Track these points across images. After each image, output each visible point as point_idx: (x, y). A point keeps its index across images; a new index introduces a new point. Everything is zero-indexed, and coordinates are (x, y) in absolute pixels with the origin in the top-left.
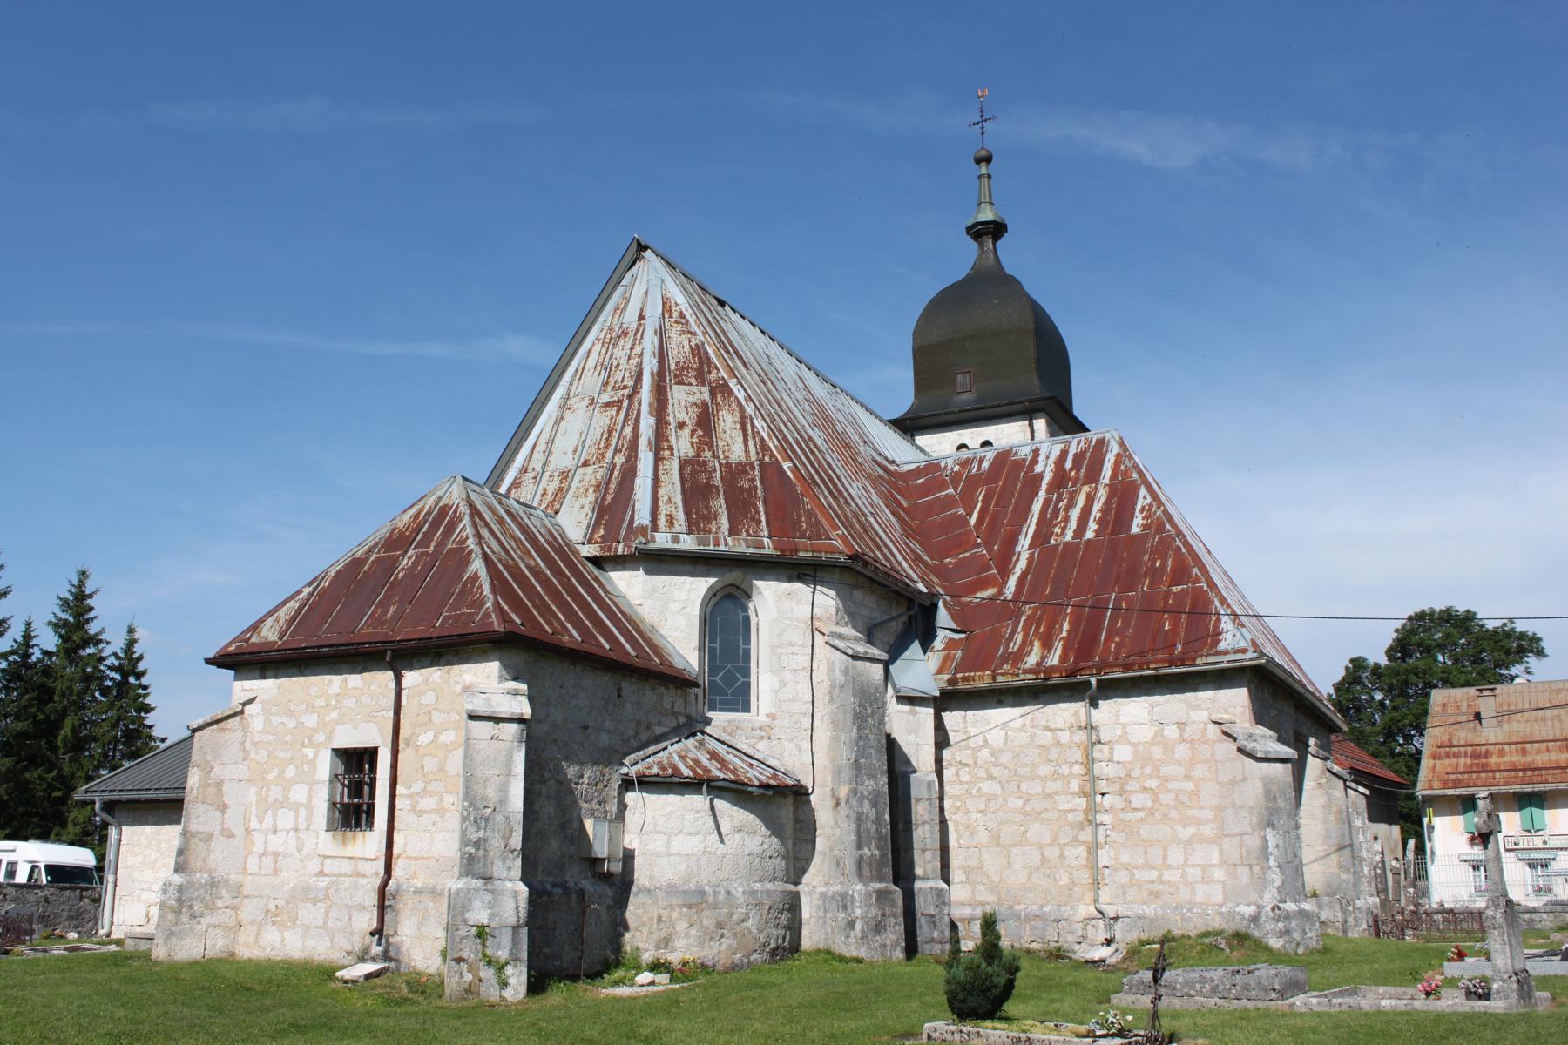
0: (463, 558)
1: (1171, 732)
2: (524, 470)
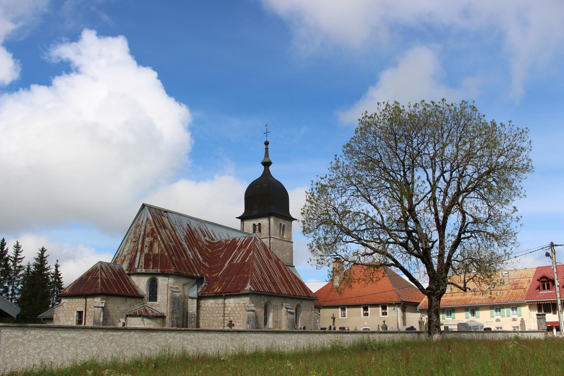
0: (97, 278)
1: (237, 305)
2: (119, 254)
